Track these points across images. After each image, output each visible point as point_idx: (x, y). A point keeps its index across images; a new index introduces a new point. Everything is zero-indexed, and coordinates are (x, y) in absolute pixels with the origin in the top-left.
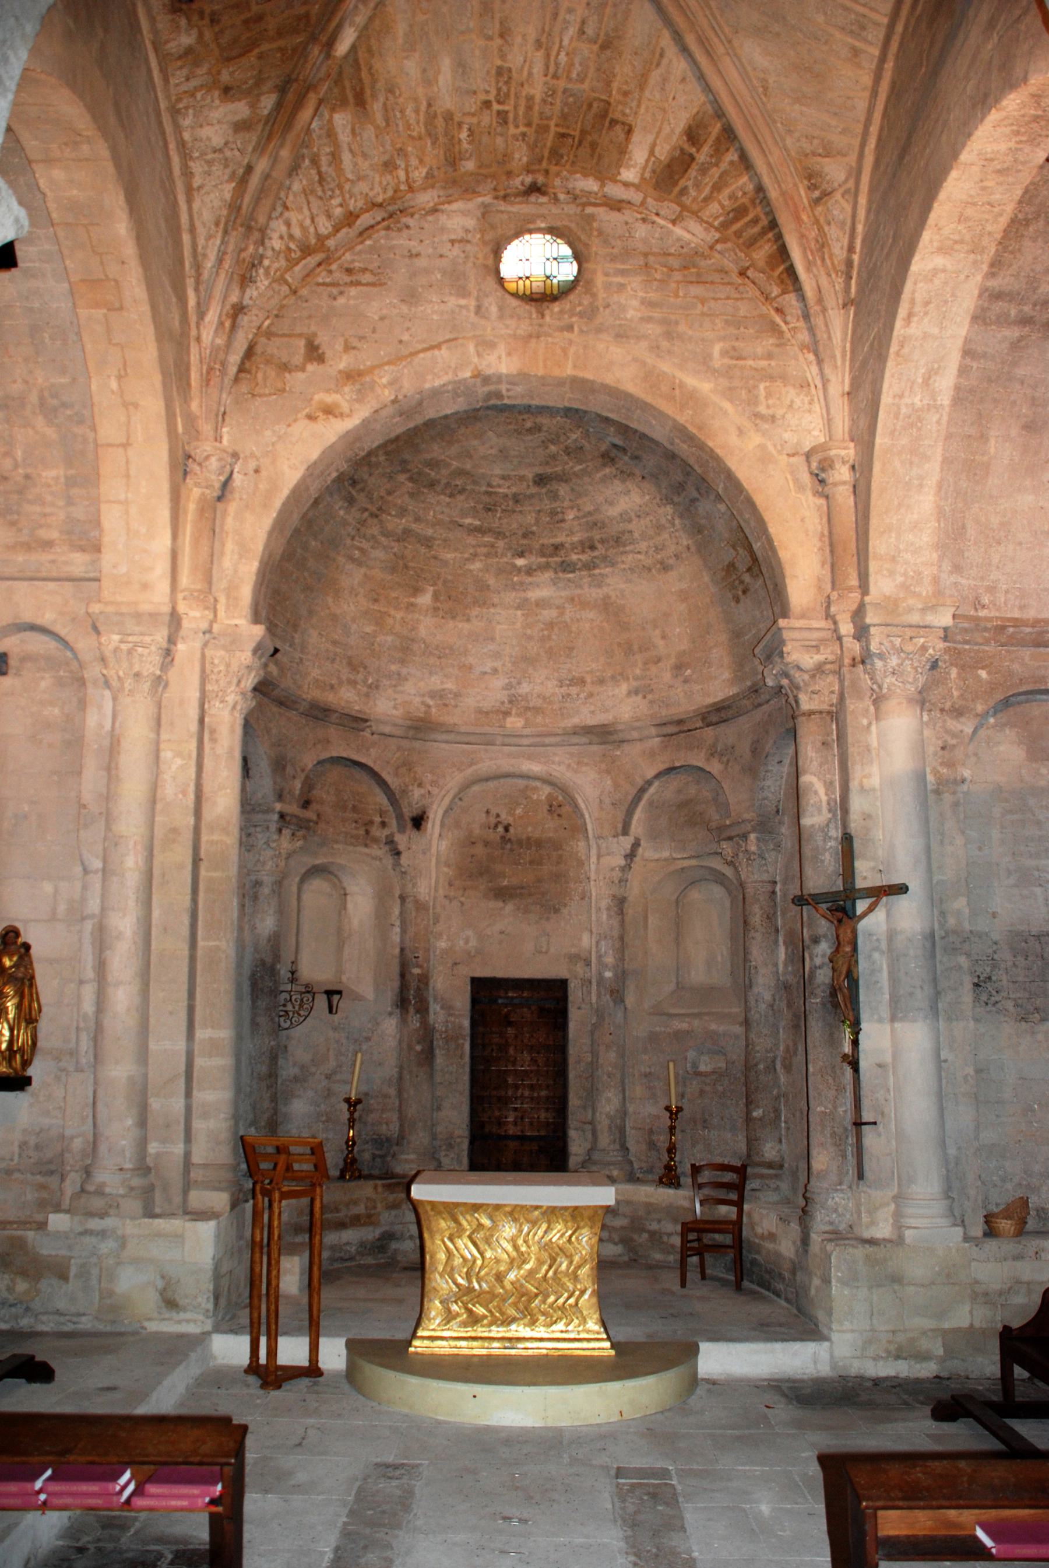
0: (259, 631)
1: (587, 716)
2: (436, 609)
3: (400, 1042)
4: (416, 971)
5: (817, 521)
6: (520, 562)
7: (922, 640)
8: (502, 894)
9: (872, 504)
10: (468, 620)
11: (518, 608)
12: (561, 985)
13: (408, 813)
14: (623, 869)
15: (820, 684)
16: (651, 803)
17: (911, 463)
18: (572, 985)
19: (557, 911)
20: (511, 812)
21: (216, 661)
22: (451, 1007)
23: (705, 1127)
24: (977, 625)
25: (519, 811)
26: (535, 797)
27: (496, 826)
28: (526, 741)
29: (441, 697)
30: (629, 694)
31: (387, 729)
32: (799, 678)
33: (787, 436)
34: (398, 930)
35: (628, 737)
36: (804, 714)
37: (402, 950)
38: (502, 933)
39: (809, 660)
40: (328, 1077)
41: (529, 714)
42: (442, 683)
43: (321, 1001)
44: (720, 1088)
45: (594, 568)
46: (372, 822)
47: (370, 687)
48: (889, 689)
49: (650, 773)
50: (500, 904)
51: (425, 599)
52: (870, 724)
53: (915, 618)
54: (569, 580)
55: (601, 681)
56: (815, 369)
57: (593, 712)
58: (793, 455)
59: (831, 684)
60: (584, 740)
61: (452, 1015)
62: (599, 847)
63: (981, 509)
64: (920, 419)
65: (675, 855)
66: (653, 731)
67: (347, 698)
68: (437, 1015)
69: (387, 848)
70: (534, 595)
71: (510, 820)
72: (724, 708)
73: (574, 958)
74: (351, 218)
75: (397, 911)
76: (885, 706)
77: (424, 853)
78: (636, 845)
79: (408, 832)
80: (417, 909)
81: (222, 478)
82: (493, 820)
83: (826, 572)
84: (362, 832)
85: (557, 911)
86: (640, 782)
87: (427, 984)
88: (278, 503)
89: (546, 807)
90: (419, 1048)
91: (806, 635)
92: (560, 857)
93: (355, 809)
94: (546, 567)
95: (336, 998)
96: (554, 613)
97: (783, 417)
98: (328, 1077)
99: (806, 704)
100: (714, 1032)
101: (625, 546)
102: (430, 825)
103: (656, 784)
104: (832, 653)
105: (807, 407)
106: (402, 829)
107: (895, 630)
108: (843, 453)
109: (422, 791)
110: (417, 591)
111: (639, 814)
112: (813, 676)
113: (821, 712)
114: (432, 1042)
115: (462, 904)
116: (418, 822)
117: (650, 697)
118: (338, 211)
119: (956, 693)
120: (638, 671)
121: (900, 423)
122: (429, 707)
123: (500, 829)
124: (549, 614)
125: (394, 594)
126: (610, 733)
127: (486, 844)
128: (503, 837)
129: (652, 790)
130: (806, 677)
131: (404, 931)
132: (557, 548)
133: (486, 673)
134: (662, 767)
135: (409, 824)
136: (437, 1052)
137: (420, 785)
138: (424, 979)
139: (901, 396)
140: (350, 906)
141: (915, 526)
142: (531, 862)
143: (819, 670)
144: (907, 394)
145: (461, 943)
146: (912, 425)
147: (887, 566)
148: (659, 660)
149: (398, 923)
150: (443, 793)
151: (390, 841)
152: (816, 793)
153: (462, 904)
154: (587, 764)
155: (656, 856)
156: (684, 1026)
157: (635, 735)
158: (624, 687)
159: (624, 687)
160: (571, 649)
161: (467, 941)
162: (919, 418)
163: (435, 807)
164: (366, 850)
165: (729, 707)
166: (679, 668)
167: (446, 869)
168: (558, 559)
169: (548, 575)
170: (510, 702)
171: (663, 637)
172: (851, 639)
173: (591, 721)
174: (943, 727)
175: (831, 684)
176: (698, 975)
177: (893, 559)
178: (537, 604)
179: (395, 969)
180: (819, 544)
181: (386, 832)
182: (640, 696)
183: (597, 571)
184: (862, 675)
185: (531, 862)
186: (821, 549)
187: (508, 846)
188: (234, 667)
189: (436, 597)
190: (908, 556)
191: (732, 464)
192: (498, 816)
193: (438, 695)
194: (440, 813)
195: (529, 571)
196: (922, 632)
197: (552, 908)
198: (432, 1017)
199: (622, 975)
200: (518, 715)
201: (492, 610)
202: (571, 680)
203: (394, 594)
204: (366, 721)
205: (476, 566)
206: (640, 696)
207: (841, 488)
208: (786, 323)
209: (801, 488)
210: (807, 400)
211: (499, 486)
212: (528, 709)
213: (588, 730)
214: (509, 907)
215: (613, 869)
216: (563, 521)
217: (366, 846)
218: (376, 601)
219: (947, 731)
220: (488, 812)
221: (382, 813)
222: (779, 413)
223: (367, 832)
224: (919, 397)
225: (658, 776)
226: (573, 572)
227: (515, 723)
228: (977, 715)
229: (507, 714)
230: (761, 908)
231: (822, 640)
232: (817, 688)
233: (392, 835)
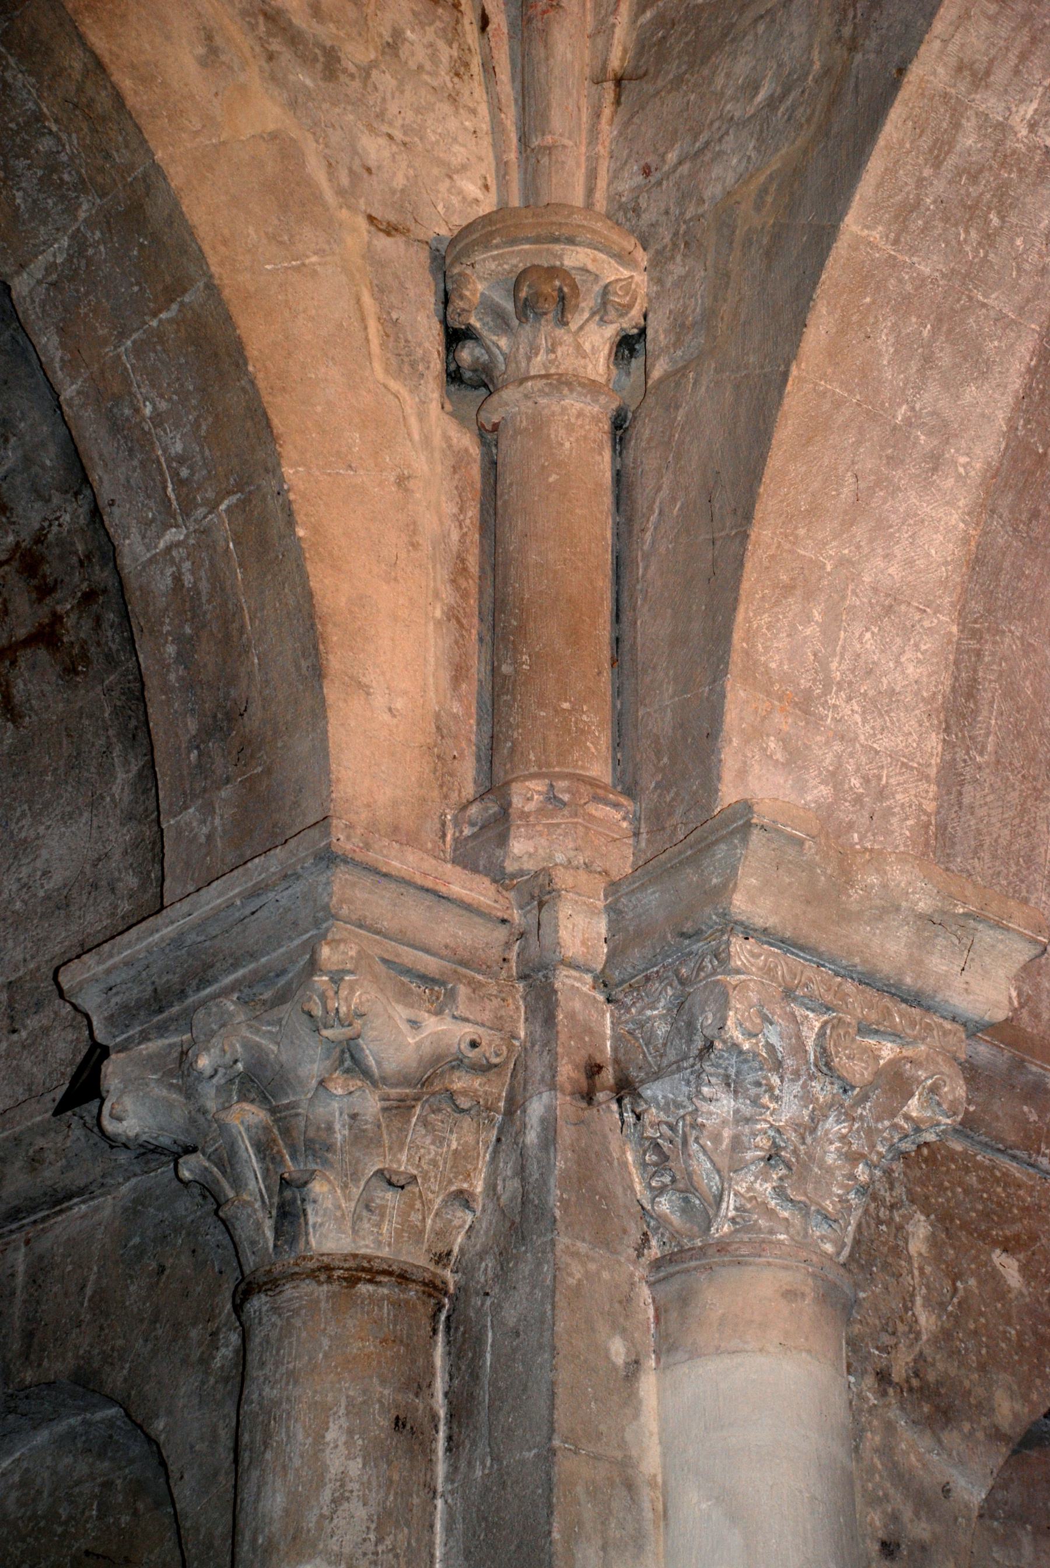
5: (450, 508)
7: (888, 1051)
9: (775, 461)
15: (420, 1150)
17: (928, 360)
24: (1019, 1065)
32: (343, 1107)
33: (374, 148)
36: (324, 1271)
39: (403, 1034)
48: (741, 1222)
52: (635, 1365)
53: (890, 947)
58: (391, 230)
59: (461, 1159)
63: (1028, 649)
64: (1003, 199)
76: (719, 1296)
83: (463, 710)
91: (414, 915)
97: (366, 72)
99: (336, 1224)
104: (498, 1025)
105: (445, 77)
107: (816, 980)
108: (612, 272)
112: (400, 1109)
113: (403, 1278)
119: (926, 1320)
121: (939, 186)
130: (371, 1104)
139: (980, 79)
141: (888, 605)
143: (423, 1089)
144: (1000, 75)
146: (973, 211)
147: (781, 721)
162: (1002, 190)
172: (585, 983)
174: (886, 1451)
175: (461, 1159)
177: (805, 705)
180: (448, 594)
184: (614, 1141)
186: (452, 615)
190: (851, 712)
191: (174, 154)
196: (899, 1015)
207: (574, 403)
209: (404, 362)
210: (446, 53)
219: (900, 1476)
222: (356, 53)
224: (1029, 110)
228: (997, 1435)
232: (403, 1164)
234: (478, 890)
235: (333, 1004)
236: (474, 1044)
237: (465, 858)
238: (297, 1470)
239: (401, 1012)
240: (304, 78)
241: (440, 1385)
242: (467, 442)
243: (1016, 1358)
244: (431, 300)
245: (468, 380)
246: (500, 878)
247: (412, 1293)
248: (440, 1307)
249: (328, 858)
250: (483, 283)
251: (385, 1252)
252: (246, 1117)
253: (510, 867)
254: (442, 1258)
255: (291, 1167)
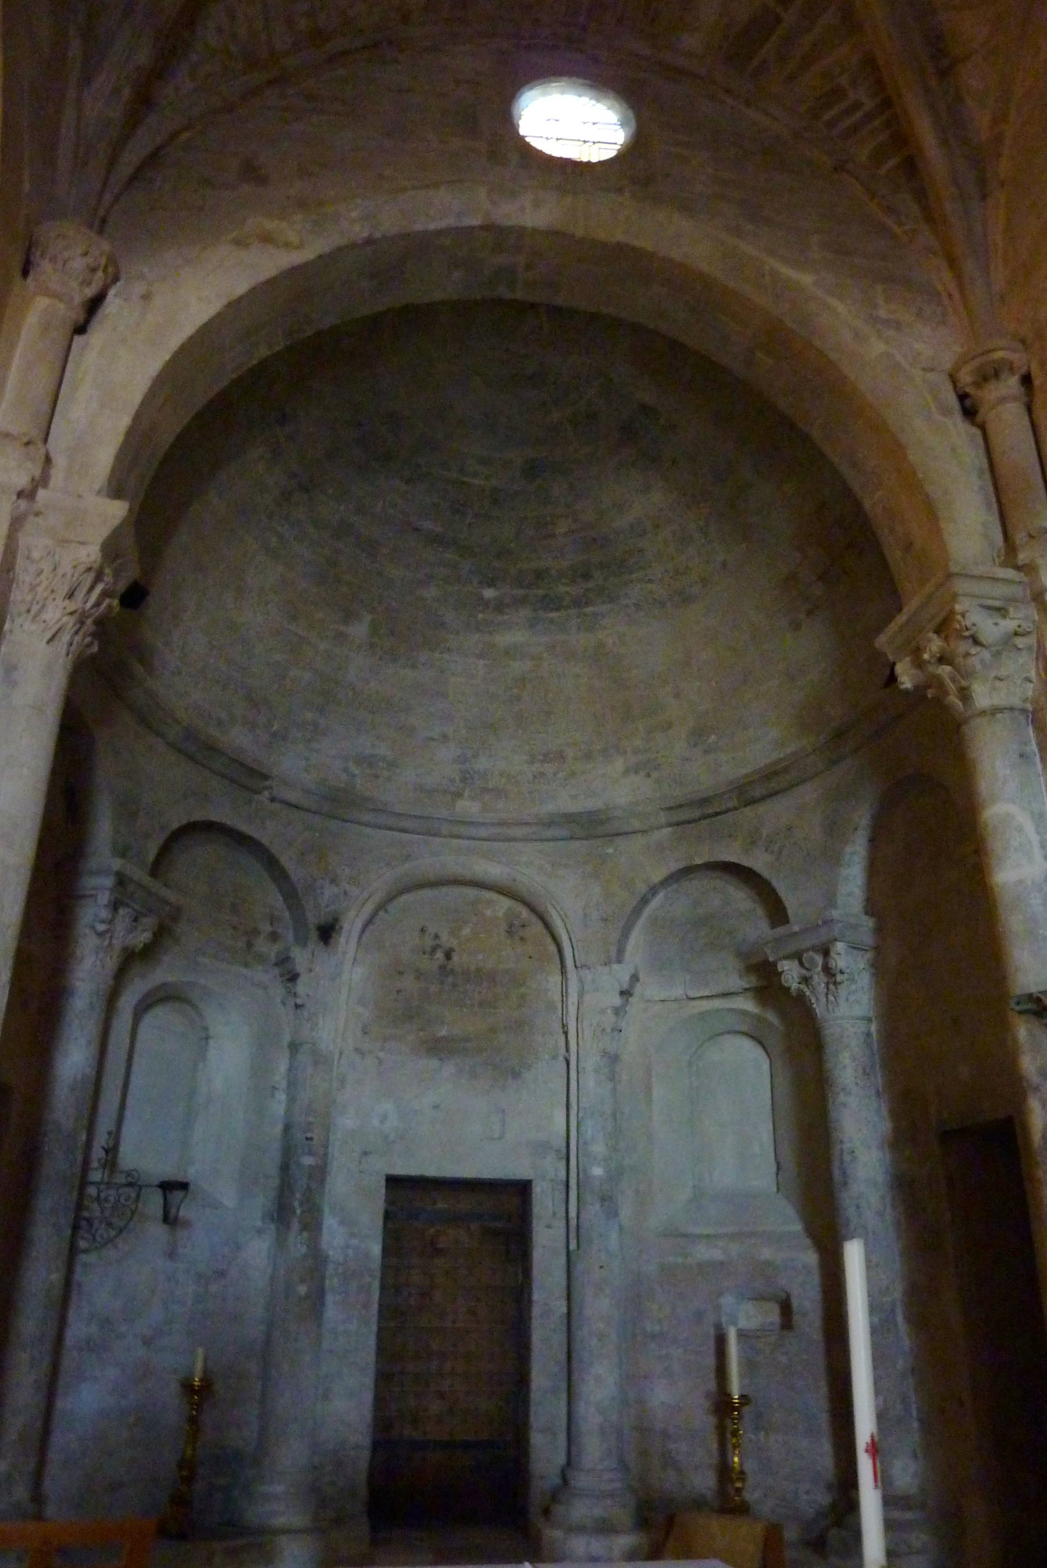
0: (118, 510)
1: (566, 800)
2: (372, 646)
3: (273, 1278)
4: (308, 1161)
6: (489, 593)
8: (438, 1048)
10: (414, 667)
11: (481, 656)
12: (522, 1189)
13: (313, 919)
14: (618, 1011)
16: (556, 1008)
18: (537, 1190)
19: (516, 1075)
20: (453, 933)
21: (36, 555)
22: (352, 1229)
23: (757, 1429)
25: (466, 931)
26: (489, 913)
27: (434, 950)
28: (483, 832)
29: (370, 765)
30: (626, 772)
31: (293, 796)
34: (281, 1096)
35: (626, 828)
36: (983, 713)
37: (287, 1128)
38: (436, 1107)
40: (147, 1342)
41: (487, 797)
42: (373, 746)
43: (154, 1202)
44: (784, 1359)
45: (587, 604)
46: (256, 932)
47: (274, 735)
49: (658, 875)
50: (434, 1063)
51: (359, 630)
54: (552, 621)
55: (588, 756)
56: (947, 275)
57: (574, 797)
60: (565, 833)
61: (352, 1235)
62: (581, 980)
65: (691, 994)
66: (663, 818)
67: (239, 739)
68: (334, 1236)
69: (276, 971)
70: (505, 639)
71: (454, 943)
72: (776, 773)
73: (541, 1148)
74: (318, 36)
75: (283, 1067)
77: (333, 979)
78: (635, 978)
79: (311, 946)
80: (316, 1063)
81: (90, 292)
82: (429, 942)
84: (241, 944)
85: (516, 1075)
86: (642, 888)
87: (322, 1182)
88: (175, 342)
89: (504, 926)
90: (302, 1289)
91: (985, 588)
92: (523, 996)
93: (234, 909)
94: (519, 602)
95: (178, 1195)
96: (529, 664)
98: (147, 1342)
100: (768, 1263)
101: (631, 572)
102: (342, 940)
103: (661, 895)
106: (302, 940)
109: (335, 890)
110: (349, 616)
111: (636, 937)
114: (323, 1278)
115: (380, 1062)
116: (327, 933)
117: (655, 775)
118: (303, 24)
120: (638, 742)
122: (354, 776)
123: (440, 955)
124: (518, 667)
125: (320, 615)
126: (602, 823)
127: (419, 975)
128: (442, 967)
129: (655, 903)
131: (292, 1100)
132: (540, 575)
133: (432, 739)
134: (674, 866)
135: (314, 935)
136: (330, 1298)
137: (334, 881)
138: (320, 1173)
140: (212, 1053)
142: (481, 1004)
145: (375, 1122)
148: (670, 725)
149: (284, 1084)
150: (365, 895)
151: (284, 961)
152: (1020, 830)
153: (380, 1062)
154: (566, 866)
155: (664, 995)
156: (717, 1255)
157: (636, 824)
158: (619, 764)
159: (619, 764)
160: (548, 713)
161: (384, 1118)
163: (352, 914)
164: (245, 971)
165: (786, 770)
166: (698, 734)
167: (360, 1010)
168: (541, 592)
169: (524, 613)
170: (464, 780)
171: (677, 696)
173: (573, 807)
176: (724, 1175)
178: (507, 653)
179: (271, 1163)
181: (276, 947)
182: (643, 773)
183: (589, 610)
185: (481, 1004)
187: (450, 979)
188: (66, 567)
189: (374, 628)
192: (437, 937)
193: (368, 761)
194: (359, 924)
195: (500, 607)
197: (509, 1071)
198: (325, 1237)
199: (615, 1175)
200: (472, 798)
201: (446, 656)
202: (546, 755)
203: (320, 615)
204: (265, 777)
205: (431, 593)
206: (643, 773)
208: (900, 224)
211: (475, 475)
212: (485, 790)
213: (570, 819)
214: (449, 1069)
215: (603, 1011)
216: (553, 536)
217: (246, 965)
218: (294, 618)
220: (423, 930)
221: (273, 920)
223: (250, 945)
225: (665, 882)
226: (557, 609)
227: (468, 807)
229: (459, 795)
230: (854, 1059)
231: (1012, 600)
232: (1003, 672)
233: (287, 949)
234: (1010, 573)
235: (963, 624)
236: (1019, 626)
237: (1004, 564)
238: (266, 988)
239: (990, 622)
240: (891, 333)
241: (1034, 742)
242: (977, 432)
243: (513, 545)
244: (950, 387)
245: (970, 412)
246: (1018, 568)
247: (1016, 713)
248: (1028, 717)
249: (950, 576)
250: (966, 377)
251: (1004, 703)
252: (945, 670)
253: (1020, 563)
254: (1025, 700)
255: (964, 683)
